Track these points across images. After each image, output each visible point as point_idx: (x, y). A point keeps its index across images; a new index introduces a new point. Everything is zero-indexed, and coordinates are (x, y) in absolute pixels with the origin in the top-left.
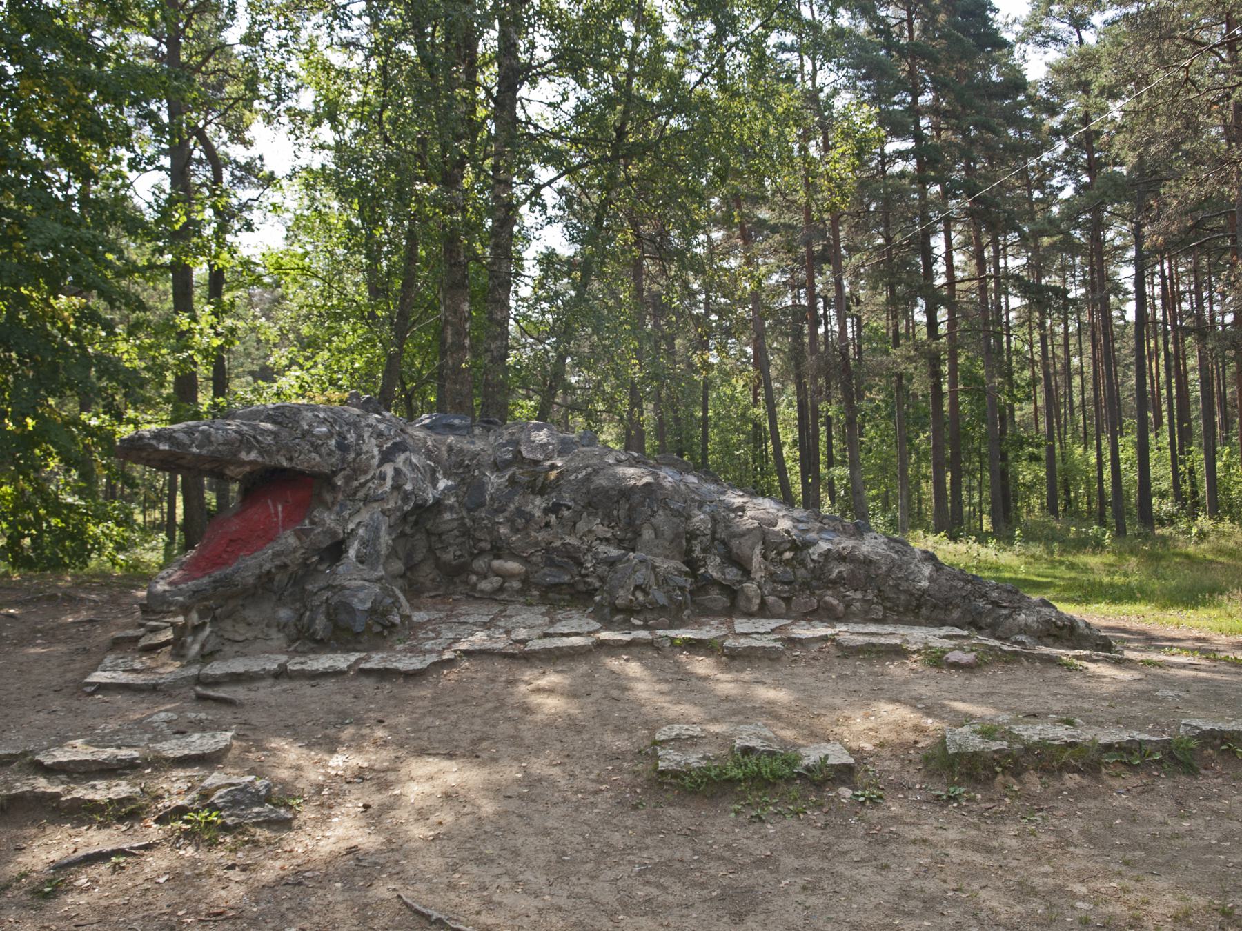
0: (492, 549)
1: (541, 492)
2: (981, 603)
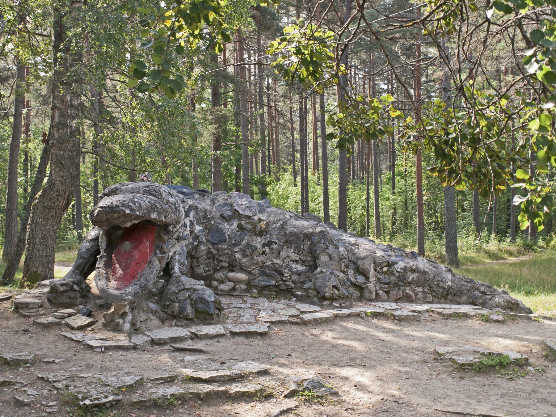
0: (228, 267)
1: (261, 234)
2: (476, 293)
